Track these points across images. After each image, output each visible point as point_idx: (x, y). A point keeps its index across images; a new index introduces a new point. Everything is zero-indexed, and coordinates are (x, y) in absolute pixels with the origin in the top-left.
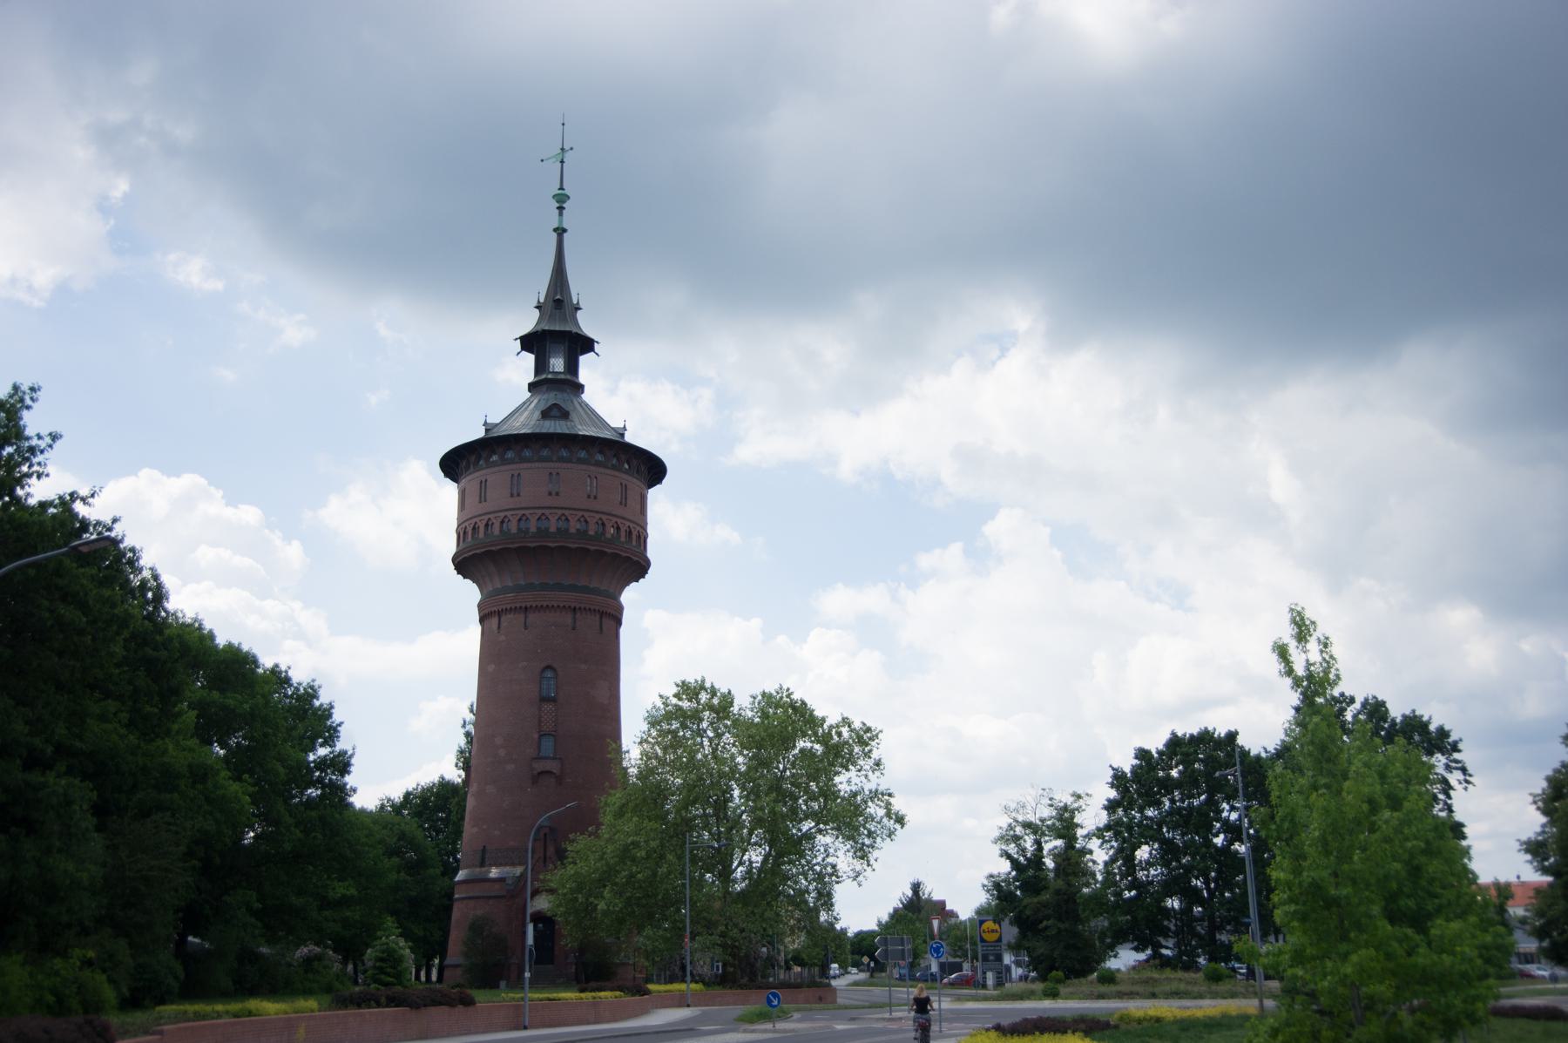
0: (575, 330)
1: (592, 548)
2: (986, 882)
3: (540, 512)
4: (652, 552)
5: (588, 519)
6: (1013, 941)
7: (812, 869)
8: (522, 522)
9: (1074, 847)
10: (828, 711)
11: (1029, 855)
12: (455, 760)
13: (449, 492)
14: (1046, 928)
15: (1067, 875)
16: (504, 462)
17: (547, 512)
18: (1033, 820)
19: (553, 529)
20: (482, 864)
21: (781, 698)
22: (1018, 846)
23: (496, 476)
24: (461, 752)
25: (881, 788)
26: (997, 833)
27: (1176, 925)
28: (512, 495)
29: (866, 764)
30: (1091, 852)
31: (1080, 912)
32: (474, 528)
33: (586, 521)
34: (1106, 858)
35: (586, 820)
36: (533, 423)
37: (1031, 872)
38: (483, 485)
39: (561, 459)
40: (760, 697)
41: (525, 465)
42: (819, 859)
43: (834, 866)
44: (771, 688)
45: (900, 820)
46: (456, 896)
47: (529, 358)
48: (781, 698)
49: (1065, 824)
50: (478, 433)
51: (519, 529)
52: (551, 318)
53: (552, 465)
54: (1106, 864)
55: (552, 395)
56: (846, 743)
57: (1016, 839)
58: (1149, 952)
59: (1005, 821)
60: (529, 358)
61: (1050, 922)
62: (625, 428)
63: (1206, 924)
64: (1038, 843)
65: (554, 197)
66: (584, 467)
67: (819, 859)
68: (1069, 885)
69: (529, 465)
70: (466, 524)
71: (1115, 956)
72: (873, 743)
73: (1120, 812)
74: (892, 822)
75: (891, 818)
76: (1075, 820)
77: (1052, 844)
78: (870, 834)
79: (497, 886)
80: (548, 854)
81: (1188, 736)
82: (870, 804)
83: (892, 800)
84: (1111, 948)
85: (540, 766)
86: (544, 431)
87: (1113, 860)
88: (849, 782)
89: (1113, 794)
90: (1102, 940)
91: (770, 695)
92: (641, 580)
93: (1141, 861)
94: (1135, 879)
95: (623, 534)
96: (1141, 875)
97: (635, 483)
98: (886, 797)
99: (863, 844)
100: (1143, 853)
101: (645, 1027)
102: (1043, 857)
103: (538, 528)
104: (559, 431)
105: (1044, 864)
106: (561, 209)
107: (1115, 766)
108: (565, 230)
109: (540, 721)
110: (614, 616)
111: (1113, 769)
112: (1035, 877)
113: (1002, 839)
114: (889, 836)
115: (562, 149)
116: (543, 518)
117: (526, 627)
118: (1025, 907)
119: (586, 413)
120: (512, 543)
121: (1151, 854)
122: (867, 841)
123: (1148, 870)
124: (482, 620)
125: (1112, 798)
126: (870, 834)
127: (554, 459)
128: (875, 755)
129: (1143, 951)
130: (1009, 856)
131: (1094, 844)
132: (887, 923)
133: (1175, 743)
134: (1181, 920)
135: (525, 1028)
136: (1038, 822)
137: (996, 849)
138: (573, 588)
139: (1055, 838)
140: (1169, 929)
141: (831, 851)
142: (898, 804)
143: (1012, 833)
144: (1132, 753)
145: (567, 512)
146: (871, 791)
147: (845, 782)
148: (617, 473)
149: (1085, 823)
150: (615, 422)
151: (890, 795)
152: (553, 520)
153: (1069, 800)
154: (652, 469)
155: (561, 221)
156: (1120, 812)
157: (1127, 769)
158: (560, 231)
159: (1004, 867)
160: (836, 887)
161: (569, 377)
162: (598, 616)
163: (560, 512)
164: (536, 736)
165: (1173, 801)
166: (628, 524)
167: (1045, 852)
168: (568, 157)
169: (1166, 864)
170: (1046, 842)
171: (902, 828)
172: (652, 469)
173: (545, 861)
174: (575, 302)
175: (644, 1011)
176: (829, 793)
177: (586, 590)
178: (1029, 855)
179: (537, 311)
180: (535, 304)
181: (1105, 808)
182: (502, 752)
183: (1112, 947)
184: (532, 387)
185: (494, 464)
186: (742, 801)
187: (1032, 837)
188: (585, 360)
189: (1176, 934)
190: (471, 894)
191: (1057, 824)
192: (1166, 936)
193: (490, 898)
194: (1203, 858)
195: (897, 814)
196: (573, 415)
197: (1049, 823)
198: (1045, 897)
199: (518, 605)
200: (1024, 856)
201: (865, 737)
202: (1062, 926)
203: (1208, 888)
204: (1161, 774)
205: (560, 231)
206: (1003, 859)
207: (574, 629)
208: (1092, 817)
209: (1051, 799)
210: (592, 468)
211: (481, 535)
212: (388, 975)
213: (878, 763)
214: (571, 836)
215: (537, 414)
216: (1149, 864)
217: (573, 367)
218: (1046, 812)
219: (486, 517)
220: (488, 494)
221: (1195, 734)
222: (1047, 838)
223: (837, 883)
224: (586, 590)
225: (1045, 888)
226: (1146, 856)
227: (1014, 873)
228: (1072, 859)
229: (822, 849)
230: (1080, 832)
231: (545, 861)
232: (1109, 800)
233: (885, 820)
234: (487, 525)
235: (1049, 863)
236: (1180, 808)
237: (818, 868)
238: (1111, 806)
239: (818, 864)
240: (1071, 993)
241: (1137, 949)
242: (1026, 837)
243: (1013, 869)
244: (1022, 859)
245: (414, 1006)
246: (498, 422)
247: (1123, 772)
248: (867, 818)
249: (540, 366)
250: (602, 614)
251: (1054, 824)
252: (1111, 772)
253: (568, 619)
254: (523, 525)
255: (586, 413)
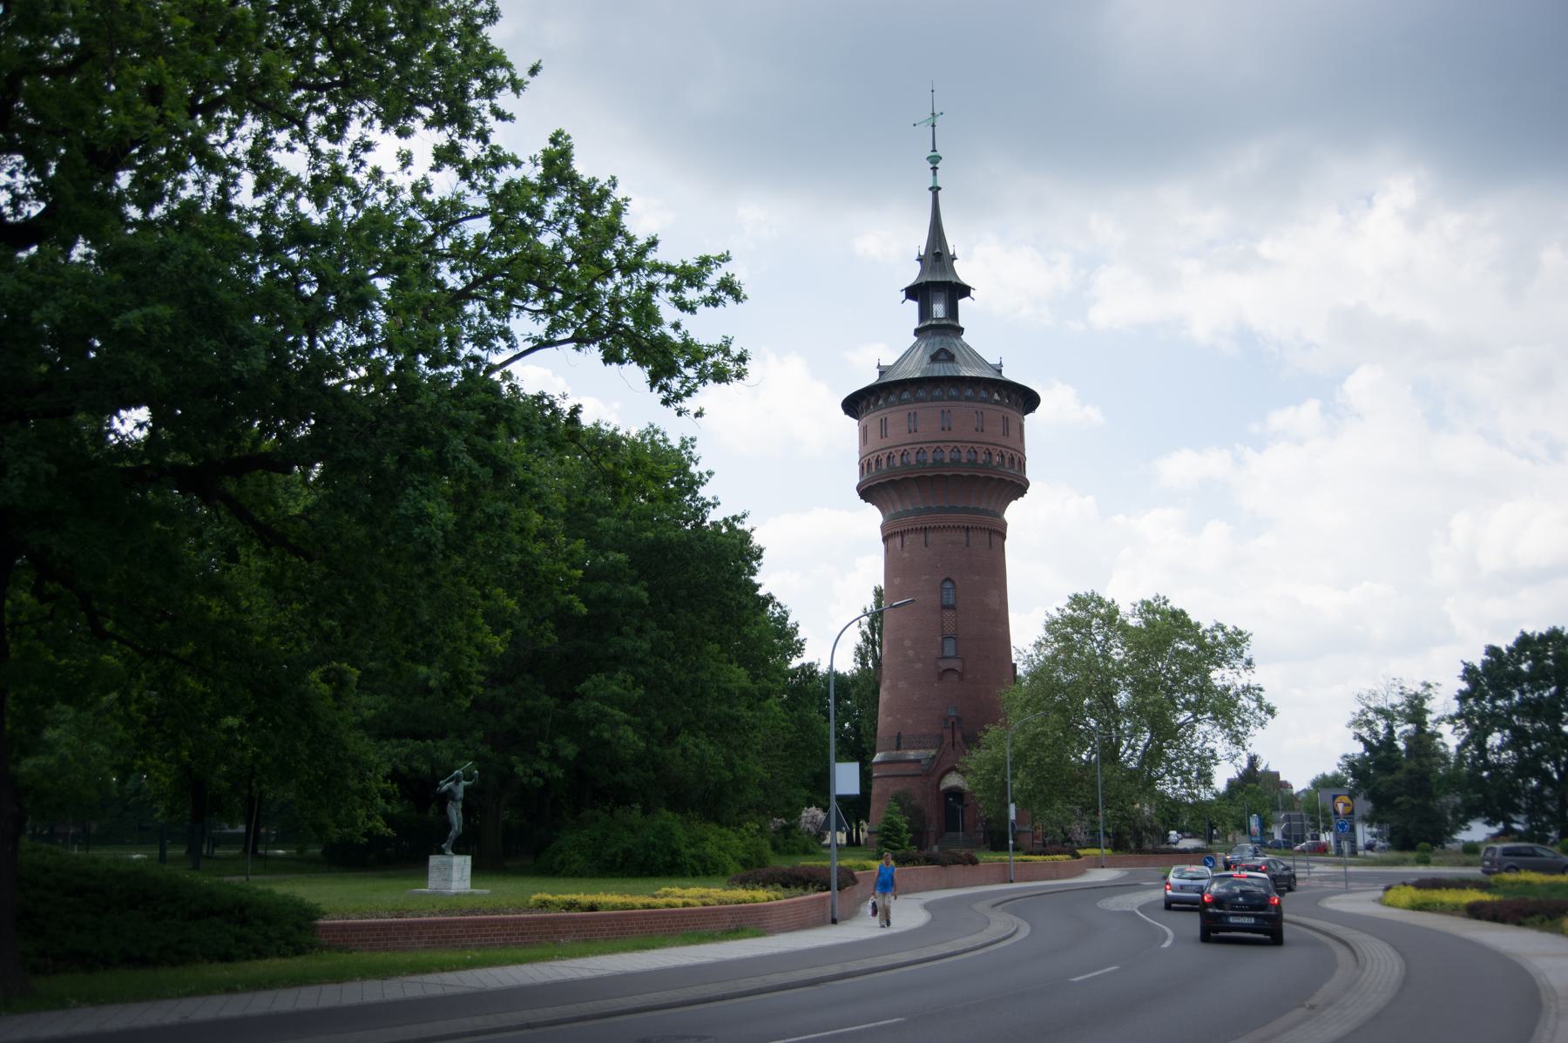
0: (954, 280)
1: (982, 475)
2: (1341, 762)
3: (935, 445)
4: (1030, 474)
5: (978, 450)
6: (1367, 814)
7: (1192, 753)
8: (920, 455)
9: (1424, 731)
10: (1203, 614)
11: (1381, 738)
12: (853, 657)
13: (852, 425)
14: (1400, 803)
15: (1419, 756)
16: (902, 402)
17: (941, 445)
18: (1384, 706)
19: (947, 460)
20: (898, 748)
21: (1159, 605)
22: (1371, 729)
23: (896, 416)
24: (859, 649)
25: (1253, 684)
26: (1351, 718)
27: (1527, 803)
28: (910, 432)
29: (1240, 664)
30: (1440, 735)
31: (1434, 790)
32: (877, 460)
33: (975, 452)
34: (1459, 742)
35: (992, 714)
36: (923, 366)
37: (1383, 754)
38: (884, 423)
39: (951, 398)
40: (1139, 605)
41: (920, 405)
42: (1198, 744)
43: (1212, 751)
44: (1149, 597)
45: (1271, 711)
46: (875, 775)
47: (913, 306)
48: (1159, 605)
49: (1416, 709)
50: (871, 378)
51: (918, 461)
52: (933, 269)
53: (943, 403)
54: (1459, 748)
55: (938, 339)
56: (1220, 644)
57: (1369, 723)
58: (1501, 825)
59: (1358, 708)
60: (913, 306)
61: (1403, 799)
62: (1001, 364)
63: (1556, 803)
64: (1390, 729)
65: (928, 158)
66: (970, 404)
67: (1198, 744)
68: (1421, 764)
69: (924, 404)
70: (870, 457)
71: (1468, 829)
72: (1243, 645)
73: (1471, 701)
74: (1263, 713)
75: (1262, 709)
76: (1425, 707)
77: (1403, 728)
78: (1244, 723)
79: (913, 766)
80: (956, 740)
81: (1537, 635)
82: (1242, 697)
83: (1262, 694)
84: (1462, 823)
85: (944, 665)
86: (936, 374)
87: (1465, 744)
88: (1223, 678)
89: (1464, 686)
90: (1454, 814)
91: (1149, 604)
92: (1020, 499)
93: (1492, 746)
94: (1486, 761)
95: (1007, 461)
96: (1492, 758)
97: (1012, 414)
98: (1257, 691)
99: (1238, 732)
100: (1495, 739)
101: (1088, 883)
102: (1395, 740)
103: (935, 460)
104: (949, 374)
105: (1395, 745)
106: (935, 169)
107: (1466, 661)
108: (939, 189)
109: (942, 627)
110: (1000, 532)
111: (1465, 664)
112: (1388, 758)
113: (1357, 723)
114: (1261, 725)
115: (933, 114)
116: (938, 450)
117: (926, 545)
118: (1380, 784)
119: (973, 359)
120: (912, 473)
121: (1502, 740)
122: (1241, 729)
123: (1500, 755)
124: (885, 539)
125: (1463, 689)
126: (1244, 723)
127: (946, 398)
128: (1246, 655)
129: (1495, 825)
130: (1362, 739)
131: (1446, 729)
132: (1224, 793)
133: (1525, 642)
134: (1532, 799)
135: (1011, 882)
136: (1389, 708)
137: (1351, 732)
138: (965, 510)
139: (1406, 723)
140: (1520, 807)
141: (1210, 737)
142: (1268, 698)
143: (1364, 718)
144: (1483, 650)
145: (959, 445)
146: (1243, 686)
147: (1220, 676)
148: (999, 408)
149: (1434, 709)
150: (992, 360)
151: (1261, 689)
152: (947, 452)
153: (1419, 689)
154: (1028, 400)
155: (935, 181)
156: (1471, 701)
157: (1478, 665)
158: (935, 190)
159: (1359, 748)
160: (1214, 768)
161: (950, 322)
162: (987, 535)
163: (952, 445)
164: (940, 639)
165: (1522, 692)
166: (1010, 451)
167: (1396, 735)
168: (938, 121)
169: (1517, 749)
170: (1398, 726)
171: (1273, 717)
172: (1028, 400)
173: (953, 745)
174: (951, 253)
175: (1082, 872)
176: (1205, 688)
177: (977, 511)
178: (1381, 738)
179: (918, 263)
180: (916, 256)
181: (1457, 698)
182: (911, 653)
183: (1464, 821)
184: (917, 332)
185: (893, 405)
186: (168, 329)
187: (1385, 722)
188: (963, 303)
189: (1528, 811)
190: (890, 773)
191: (1408, 710)
192: (1517, 812)
193: (909, 776)
194: (1554, 745)
195: (1268, 706)
196: (958, 357)
197: (1400, 709)
198: (1399, 775)
199: (919, 527)
200: (1377, 739)
201: (1237, 640)
202: (1415, 802)
203: (1558, 771)
204: (1510, 668)
205: (935, 190)
206: (1357, 742)
207: (968, 545)
208: (1443, 703)
209: (1401, 688)
210: (979, 404)
211: (884, 466)
212: (894, 841)
213: (1249, 663)
214: (986, 727)
215: (927, 358)
216: (1501, 748)
217: (953, 312)
218: (1397, 700)
219: (888, 451)
220: (888, 431)
221: (1544, 633)
222: (1398, 723)
223: (1216, 764)
224: (977, 511)
225: (1399, 767)
226: (1498, 742)
227: (1367, 754)
228: (1423, 742)
229: (1201, 736)
230: (1429, 718)
231: (953, 745)
232: (1460, 691)
233: (1257, 711)
234: (889, 457)
235: (1401, 745)
236: (1529, 699)
237: (1196, 751)
238: (1462, 697)
239: (1196, 748)
240: (1440, 861)
241: (1489, 824)
242: (1378, 722)
243: (1366, 750)
244: (1374, 741)
245: (944, 864)
246: (891, 364)
247: (1474, 667)
248: (1240, 709)
249: (925, 313)
250: (991, 532)
251: (1404, 710)
252: (1463, 667)
253: (962, 537)
254: (920, 457)
255: (973, 359)
